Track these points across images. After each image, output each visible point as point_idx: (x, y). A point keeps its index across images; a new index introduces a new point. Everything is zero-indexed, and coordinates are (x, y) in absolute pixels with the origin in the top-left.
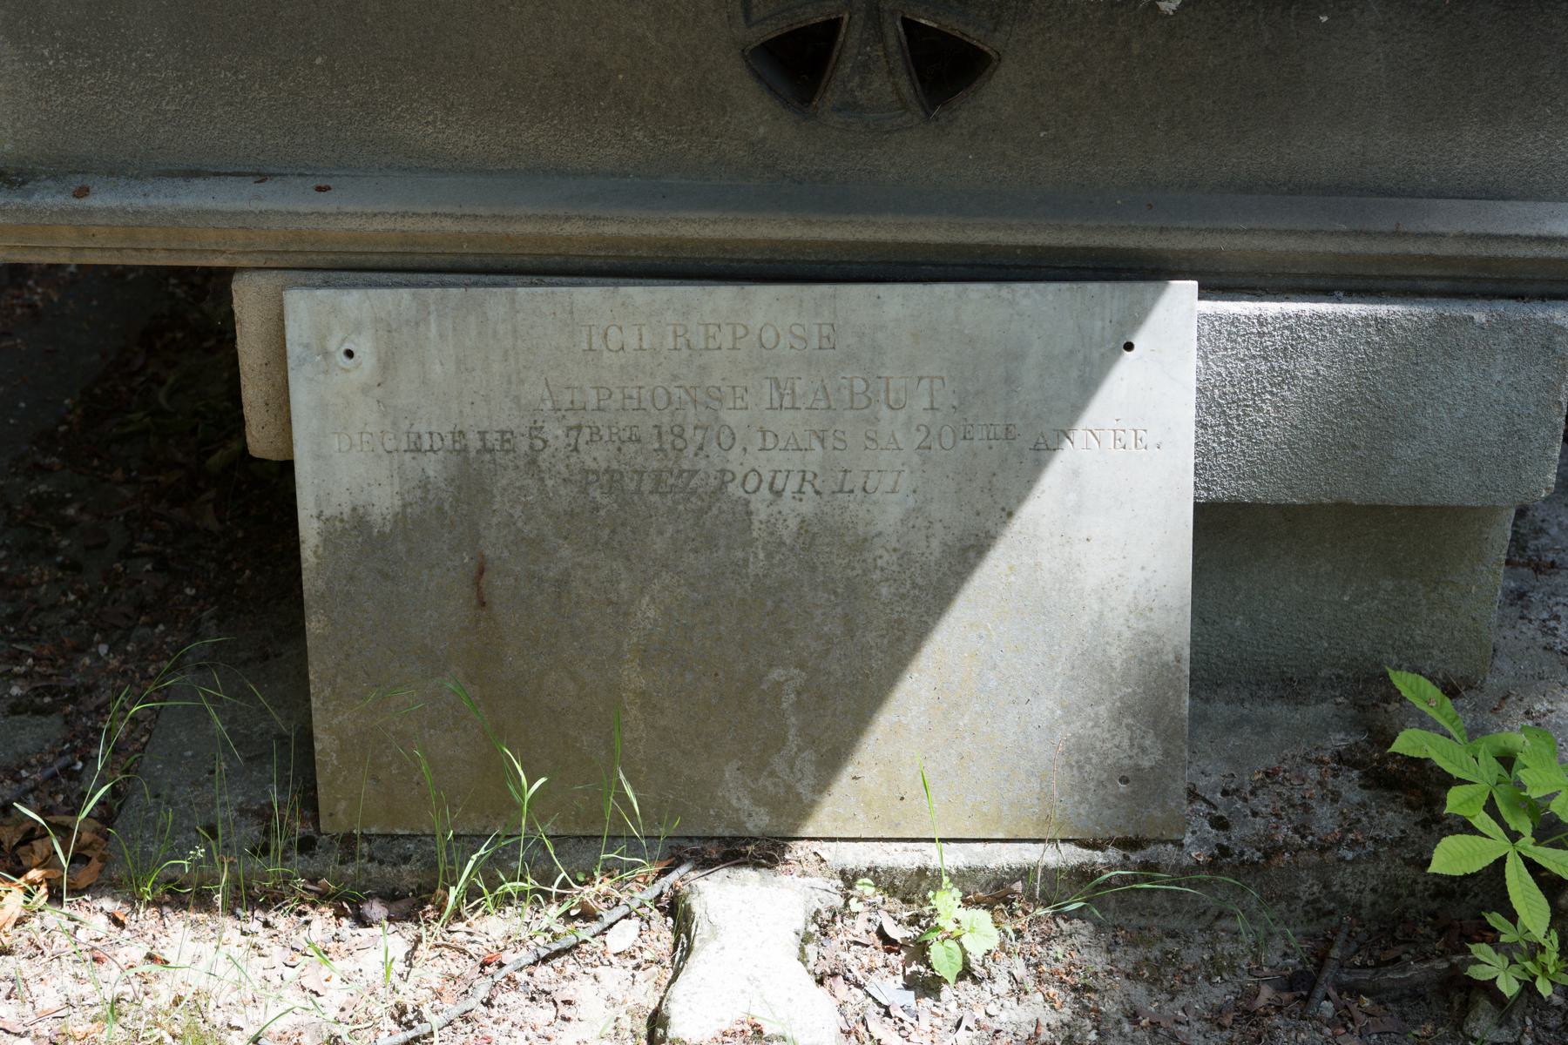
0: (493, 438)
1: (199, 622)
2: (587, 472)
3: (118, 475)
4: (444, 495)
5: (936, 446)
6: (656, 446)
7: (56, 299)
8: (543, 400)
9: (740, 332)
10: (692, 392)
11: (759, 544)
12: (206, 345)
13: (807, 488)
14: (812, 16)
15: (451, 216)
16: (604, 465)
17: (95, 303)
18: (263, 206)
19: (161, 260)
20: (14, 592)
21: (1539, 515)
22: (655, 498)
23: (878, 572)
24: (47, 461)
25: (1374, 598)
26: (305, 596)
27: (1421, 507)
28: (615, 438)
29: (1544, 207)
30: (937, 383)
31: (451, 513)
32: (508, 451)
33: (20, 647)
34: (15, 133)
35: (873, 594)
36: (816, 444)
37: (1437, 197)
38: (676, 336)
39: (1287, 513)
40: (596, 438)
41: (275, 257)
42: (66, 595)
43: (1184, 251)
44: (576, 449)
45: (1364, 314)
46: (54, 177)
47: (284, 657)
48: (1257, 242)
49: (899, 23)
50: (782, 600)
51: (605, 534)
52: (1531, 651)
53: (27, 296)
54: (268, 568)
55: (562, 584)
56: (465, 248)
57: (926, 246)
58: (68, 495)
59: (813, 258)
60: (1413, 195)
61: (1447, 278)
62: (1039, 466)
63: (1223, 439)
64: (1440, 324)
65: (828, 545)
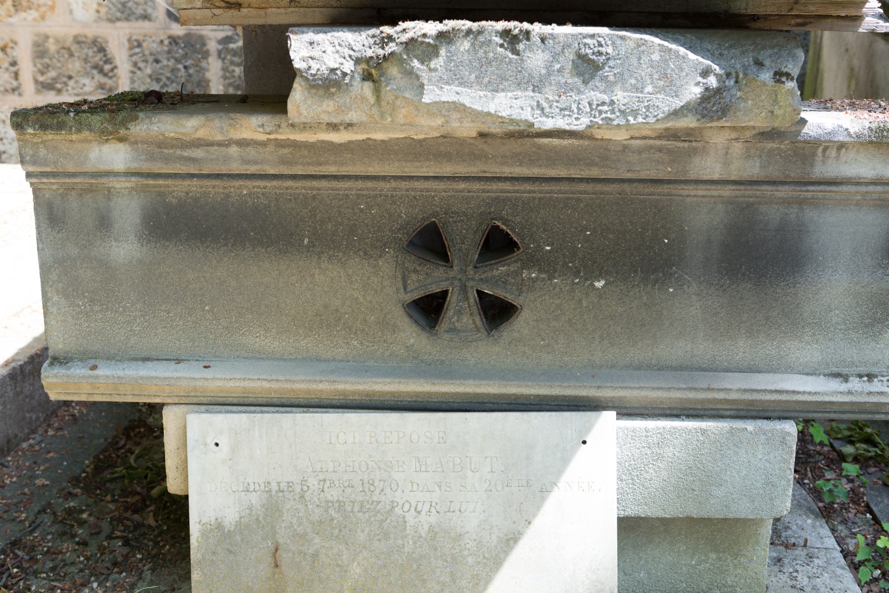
0: (283, 486)
1: (142, 571)
2: (328, 502)
3: (109, 498)
4: (259, 513)
5: (494, 490)
6: (361, 489)
7: (85, 412)
8: (308, 467)
9: (401, 435)
10: (378, 463)
11: (410, 537)
12: (155, 434)
13: (433, 510)
14: (435, 289)
15: (266, 380)
16: (336, 498)
17: (103, 414)
18: (178, 375)
19: (130, 399)
20: (54, 556)
21: (787, 520)
22: (360, 514)
23: (467, 551)
24: (75, 491)
25: (707, 563)
26: (192, 561)
27: (726, 519)
28: (341, 485)
29: (778, 376)
30: (495, 460)
31: (263, 521)
32: (290, 492)
33: (55, 584)
34: (64, 340)
35: (464, 562)
36: (437, 489)
37: (727, 372)
38: (371, 437)
39: (665, 523)
40: (332, 485)
41: (184, 398)
42: (79, 557)
43: (609, 397)
44: (323, 491)
45: (695, 427)
46: (81, 360)
47: (182, 590)
48: (644, 393)
49: (475, 292)
50: (421, 565)
51: (336, 532)
52: (785, 588)
53: (71, 410)
54: (178, 545)
55: (315, 556)
56: (273, 395)
57: (489, 395)
58: (84, 508)
59: (436, 400)
60: (716, 370)
61: (734, 409)
62: (543, 499)
63: (631, 486)
64: (731, 431)
65: (442, 537)
